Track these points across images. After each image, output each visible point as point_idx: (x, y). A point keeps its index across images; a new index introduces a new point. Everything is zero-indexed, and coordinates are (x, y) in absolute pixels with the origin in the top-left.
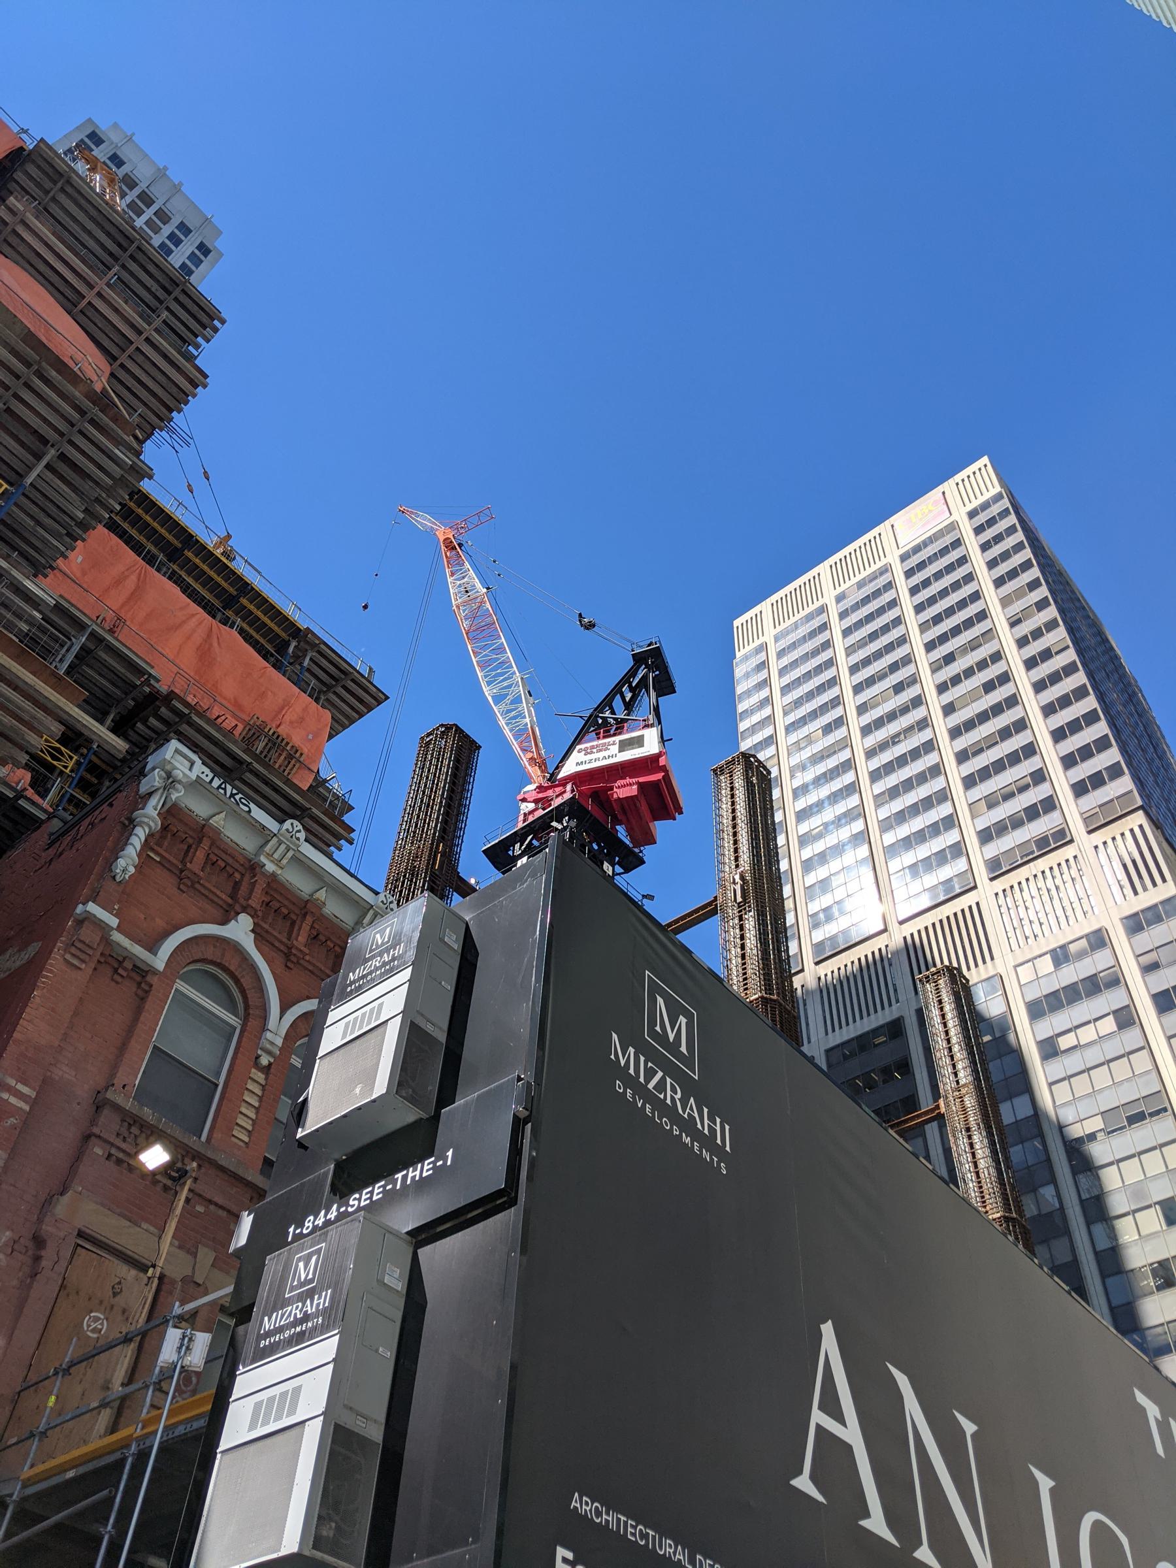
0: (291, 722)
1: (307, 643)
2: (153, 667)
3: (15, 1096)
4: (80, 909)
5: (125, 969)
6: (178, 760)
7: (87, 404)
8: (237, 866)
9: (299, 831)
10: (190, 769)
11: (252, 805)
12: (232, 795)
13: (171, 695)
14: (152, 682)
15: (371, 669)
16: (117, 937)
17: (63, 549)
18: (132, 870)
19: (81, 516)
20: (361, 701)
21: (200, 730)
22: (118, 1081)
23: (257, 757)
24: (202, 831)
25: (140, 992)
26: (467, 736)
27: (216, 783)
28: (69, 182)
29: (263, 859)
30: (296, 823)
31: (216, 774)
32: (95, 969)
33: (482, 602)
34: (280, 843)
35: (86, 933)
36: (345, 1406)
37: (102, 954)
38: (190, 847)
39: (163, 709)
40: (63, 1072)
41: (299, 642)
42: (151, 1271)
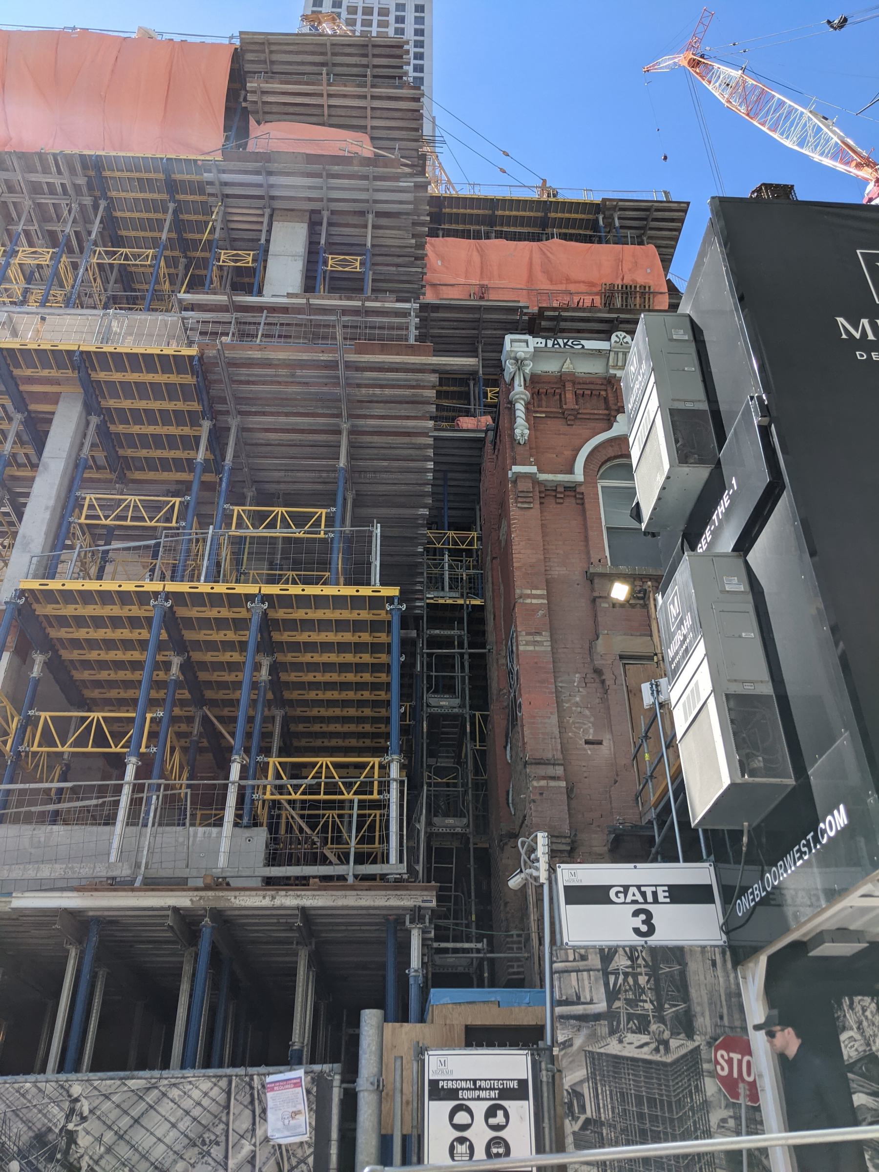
0: (630, 270)
1: (609, 209)
2: (519, 302)
3: (534, 598)
4: (510, 474)
5: (561, 493)
6: (519, 346)
7: (364, 170)
8: (598, 387)
9: (625, 337)
10: (528, 346)
11: (583, 342)
12: (565, 344)
13: (542, 310)
14: (525, 311)
15: (665, 192)
16: (543, 477)
17: (420, 270)
18: (527, 432)
19: (413, 241)
20: (672, 220)
21: (573, 319)
22: (594, 559)
23: (619, 311)
24: (562, 379)
25: (579, 501)
26: (778, 186)
27: (550, 343)
28: (270, 44)
29: (612, 371)
30: (619, 333)
31: (547, 338)
32: (541, 503)
33: (744, 82)
34: (617, 353)
35: (523, 486)
36: (729, 680)
37: (540, 492)
38: (560, 395)
39: (543, 323)
40: (558, 571)
41: (604, 213)
42: (655, 658)
